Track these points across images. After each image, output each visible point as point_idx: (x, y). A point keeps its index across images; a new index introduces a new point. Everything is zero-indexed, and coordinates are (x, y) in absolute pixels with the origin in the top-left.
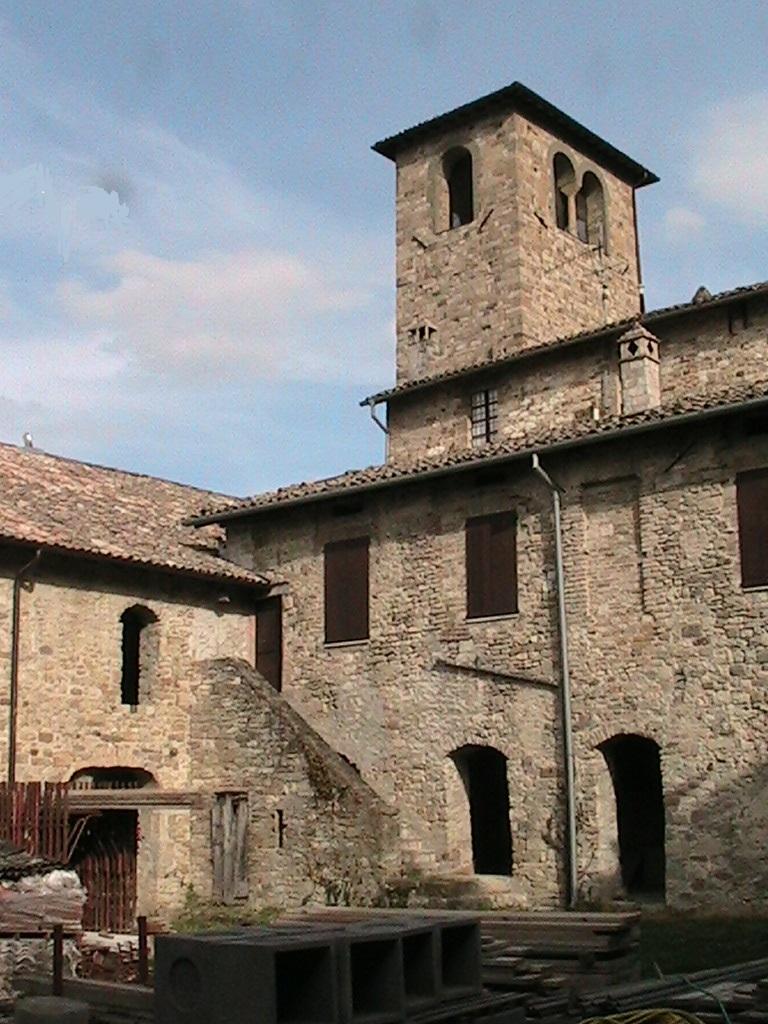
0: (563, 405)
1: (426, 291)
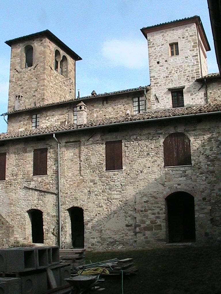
0: (58, 120)
1: (18, 84)
